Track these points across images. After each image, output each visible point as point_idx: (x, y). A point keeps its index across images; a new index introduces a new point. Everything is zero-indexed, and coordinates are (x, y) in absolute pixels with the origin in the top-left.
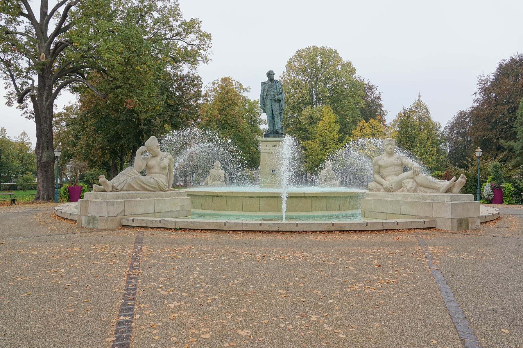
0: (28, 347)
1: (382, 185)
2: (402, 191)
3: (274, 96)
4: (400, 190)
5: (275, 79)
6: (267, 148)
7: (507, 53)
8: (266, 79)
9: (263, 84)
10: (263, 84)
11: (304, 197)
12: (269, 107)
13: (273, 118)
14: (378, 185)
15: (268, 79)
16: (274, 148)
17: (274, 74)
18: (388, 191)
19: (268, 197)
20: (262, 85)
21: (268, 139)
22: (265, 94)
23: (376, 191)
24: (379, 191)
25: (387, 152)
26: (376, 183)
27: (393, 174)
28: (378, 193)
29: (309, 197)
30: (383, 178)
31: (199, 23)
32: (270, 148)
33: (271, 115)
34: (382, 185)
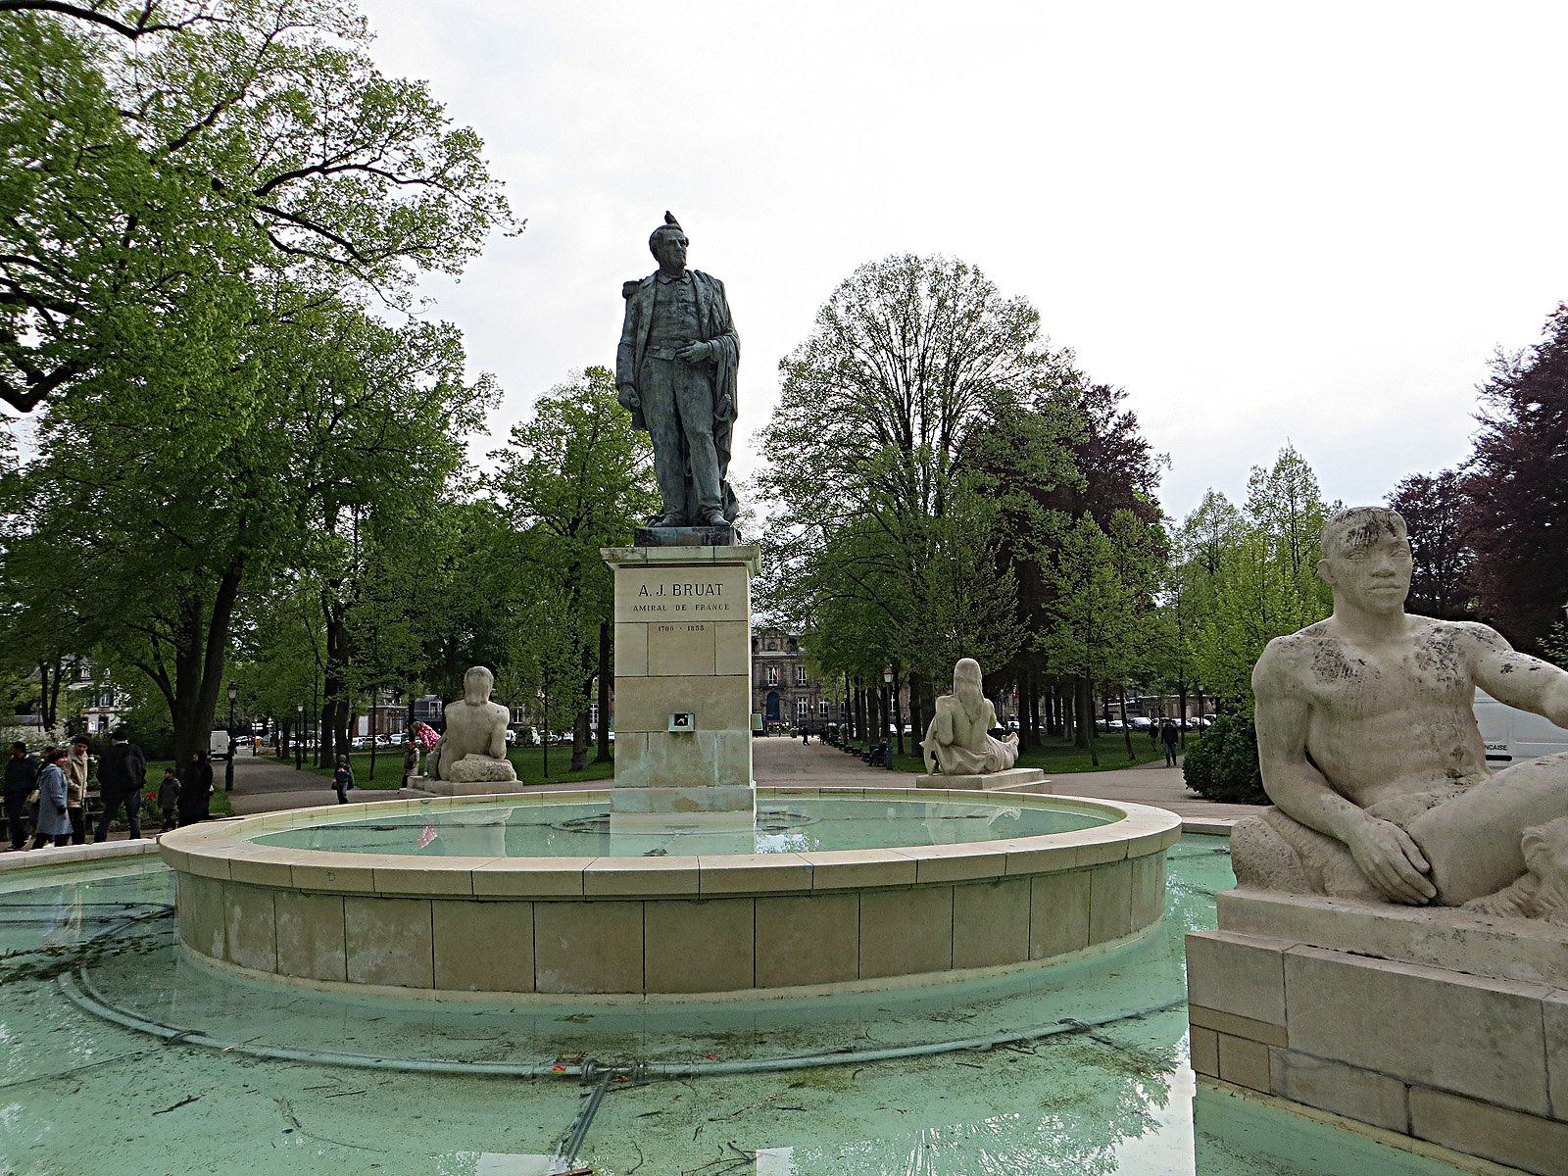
0: (206, 1171)
1: (1343, 846)
2: (1529, 911)
3: (686, 341)
4: (1502, 899)
5: (691, 265)
6: (646, 601)
7: (1525, 338)
8: (647, 266)
9: (630, 290)
10: (630, 290)
11: (809, 894)
12: (659, 401)
13: (682, 451)
14: (1305, 839)
15: (656, 266)
16: (679, 600)
17: (685, 243)
18: (1395, 900)
19: (587, 900)
20: (626, 295)
21: (654, 553)
22: (642, 335)
23: (1294, 889)
24: (1320, 888)
25: (1353, 602)
26: (1290, 828)
27: (1419, 768)
28: (1312, 902)
29: (843, 892)
30: (1348, 794)
31: (479, 145)
32: (657, 602)
33: (672, 439)
34: (1343, 846)
